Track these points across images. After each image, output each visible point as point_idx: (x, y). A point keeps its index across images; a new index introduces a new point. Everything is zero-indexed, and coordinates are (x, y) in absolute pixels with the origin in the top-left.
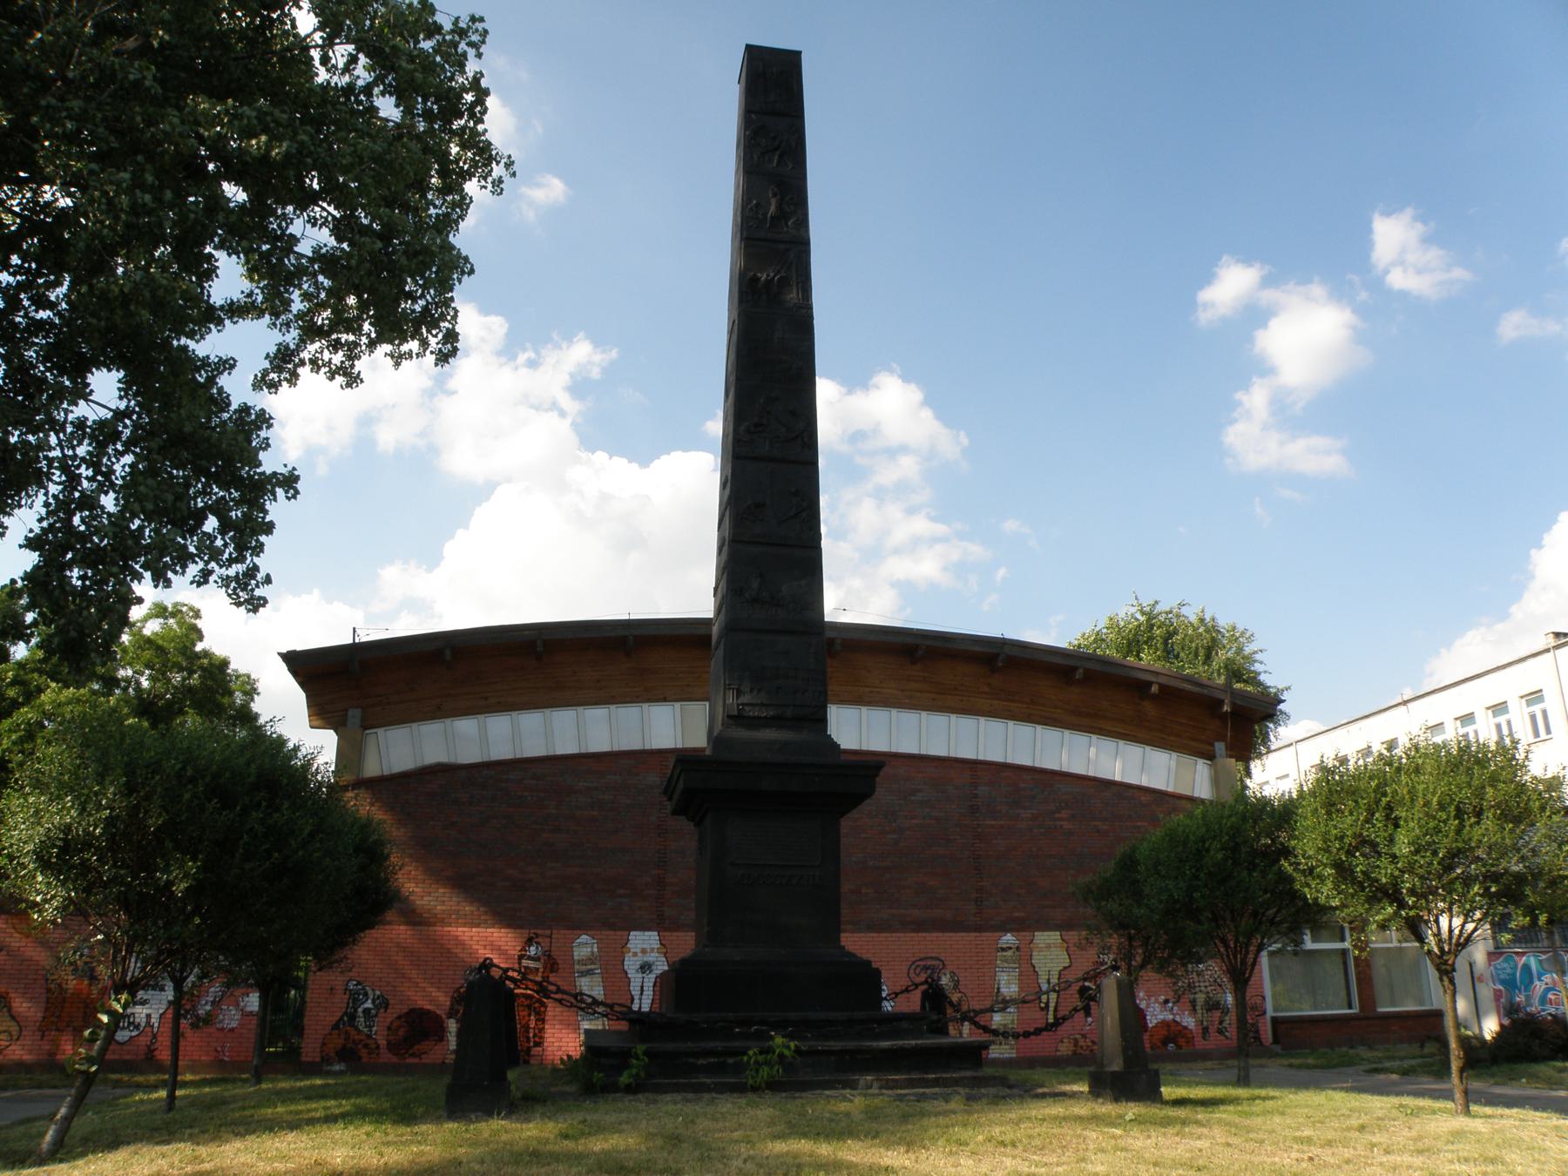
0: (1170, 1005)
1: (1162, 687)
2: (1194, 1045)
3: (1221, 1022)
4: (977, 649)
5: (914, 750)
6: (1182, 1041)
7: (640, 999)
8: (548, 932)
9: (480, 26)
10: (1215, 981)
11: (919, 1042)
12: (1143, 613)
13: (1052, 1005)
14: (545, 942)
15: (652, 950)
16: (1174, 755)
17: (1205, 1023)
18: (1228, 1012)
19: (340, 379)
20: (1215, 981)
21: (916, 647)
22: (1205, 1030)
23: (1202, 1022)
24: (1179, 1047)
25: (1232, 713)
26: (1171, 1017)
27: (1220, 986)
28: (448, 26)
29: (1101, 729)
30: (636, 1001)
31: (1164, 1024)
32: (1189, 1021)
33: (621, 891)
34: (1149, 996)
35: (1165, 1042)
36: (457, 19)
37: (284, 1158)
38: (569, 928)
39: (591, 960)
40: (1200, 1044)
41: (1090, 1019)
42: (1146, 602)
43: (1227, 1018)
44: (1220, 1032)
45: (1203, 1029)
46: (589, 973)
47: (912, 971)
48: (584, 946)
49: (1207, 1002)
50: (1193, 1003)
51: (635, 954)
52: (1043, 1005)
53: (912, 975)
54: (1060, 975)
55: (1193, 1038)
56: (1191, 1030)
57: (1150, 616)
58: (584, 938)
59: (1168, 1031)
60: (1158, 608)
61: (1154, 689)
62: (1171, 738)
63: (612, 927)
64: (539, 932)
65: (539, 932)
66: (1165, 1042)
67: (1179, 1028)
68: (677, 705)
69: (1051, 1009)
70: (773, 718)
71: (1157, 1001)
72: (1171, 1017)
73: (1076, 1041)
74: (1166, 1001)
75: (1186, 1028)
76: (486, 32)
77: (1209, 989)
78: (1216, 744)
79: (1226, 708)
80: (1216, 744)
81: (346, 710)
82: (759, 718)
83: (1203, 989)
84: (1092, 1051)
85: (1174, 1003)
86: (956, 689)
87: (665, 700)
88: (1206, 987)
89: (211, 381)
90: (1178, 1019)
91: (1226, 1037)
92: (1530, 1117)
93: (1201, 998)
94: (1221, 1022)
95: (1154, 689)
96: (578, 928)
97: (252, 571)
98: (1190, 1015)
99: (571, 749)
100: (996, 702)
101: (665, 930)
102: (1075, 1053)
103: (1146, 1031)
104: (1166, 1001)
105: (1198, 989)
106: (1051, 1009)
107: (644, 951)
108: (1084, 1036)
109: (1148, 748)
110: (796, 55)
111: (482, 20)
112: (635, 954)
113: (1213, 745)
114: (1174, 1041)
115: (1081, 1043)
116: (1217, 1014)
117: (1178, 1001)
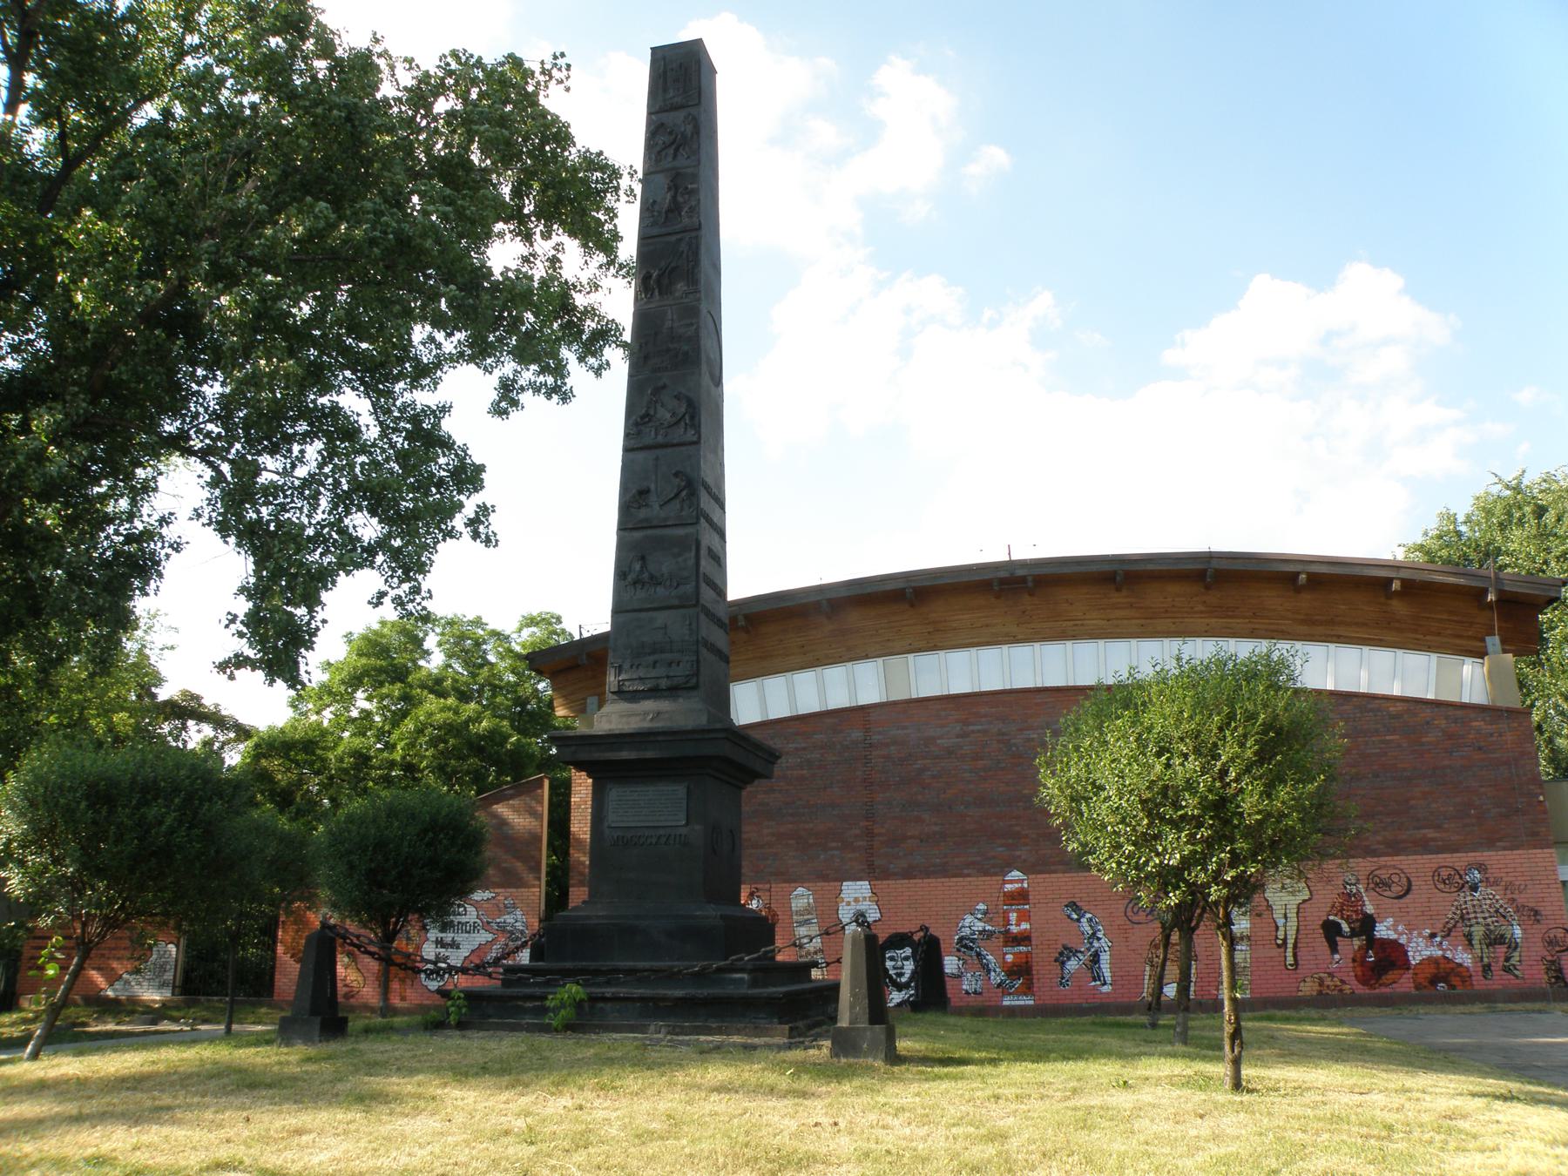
0: (1438, 939)
1: (1405, 583)
2: (1472, 985)
3: (1507, 959)
4: (1190, 567)
5: (1030, 684)
6: (1455, 981)
7: (1285, 926)
8: (768, 886)
9: (560, 62)
10: (1497, 911)
11: (711, 991)
12: (1508, 487)
13: (1291, 942)
14: (765, 896)
15: (864, 898)
16: (1434, 657)
17: (1486, 960)
18: (1516, 947)
19: (555, 397)
20: (1497, 911)
21: (1115, 573)
22: (1487, 969)
23: (1482, 958)
24: (1452, 987)
25: (1498, 601)
26: (1440, 953)
27: (1504, 917)
28: (537, 68)
29: (1339, 637)
30: (1282, 929)
31: (1431, 960)
32: (1464, 958)
33: (834, 844)
34: (1411, 931)
35: (1434, 981)
36: (542, 63)
37: (1471, 1083)
38: (785, 881)
39: (808, 911)
40: (1479, 983)
41: (1337, 957)
42: (1509, 476)
43: (1516, 954)
44: (1507, 970)
45: (1484, 966)
46: (807, 922)
47: (1129, 909)
48: (801, 898)
49: (1486, 936)
50: (1469, 938)
51: (848, 904)
52: (1279, 942)
53: (1129, 913)
54: (1298, 908)
55: (1471, 976)
56: (1467, 968)
57: (1517, 489)
58: (800, 890)
59: (1438, 968)
60: (1526, 482)
61: (1396, 586)
62: (1428, 638)
63: (825, 878)
64: (759, 886)
65: (759, 886)
66: (1434, 981)
67: (1451, 965)
68: (880, 660)
69: (1290, 946)
70: (650, 690)
71: (1420, 935)
72: (1440, 953)
73: (1321, 980)
74: (1433, 936)
75: (1460, 965)
76: (568, 67)
77: (1489, 920)
78: (1488, 639)
79: (1491, 597)
80: (1488, 639)
81: (585, 699)
82: (636, 691)
83: (1480, 920)
84: (1341, 990)
85: (1443, 937)
86: (1166, 612)
87: (867, 657)
88: (1485, 918)
89: (436, 426)
90: (1449, 954)
91: (1516, 976)
92: (1048, 1077)
93: (1478, 932)
94: (1507, 959)
95: (1396, 586)
96: (795, 881)
97: (416, 590)
98: (1465, 950)
99: (815, 707)
100: (1214, 620)
101: (877, 879)
102: (1320, 993)
103: (1408, 969)
104: (1433, 936)
105: (1474, 921)
106: (1290, 946)
107: (856, 900)
108: (1331, 975)
109: (1400, 652)
110: (653, 49)
111: (563, 55)
112: (848, 904)
113: (1483, 640)
114: (1445, 979)
115: (1328, 982)
116: (1502, 949)
117: (1448, 935)
